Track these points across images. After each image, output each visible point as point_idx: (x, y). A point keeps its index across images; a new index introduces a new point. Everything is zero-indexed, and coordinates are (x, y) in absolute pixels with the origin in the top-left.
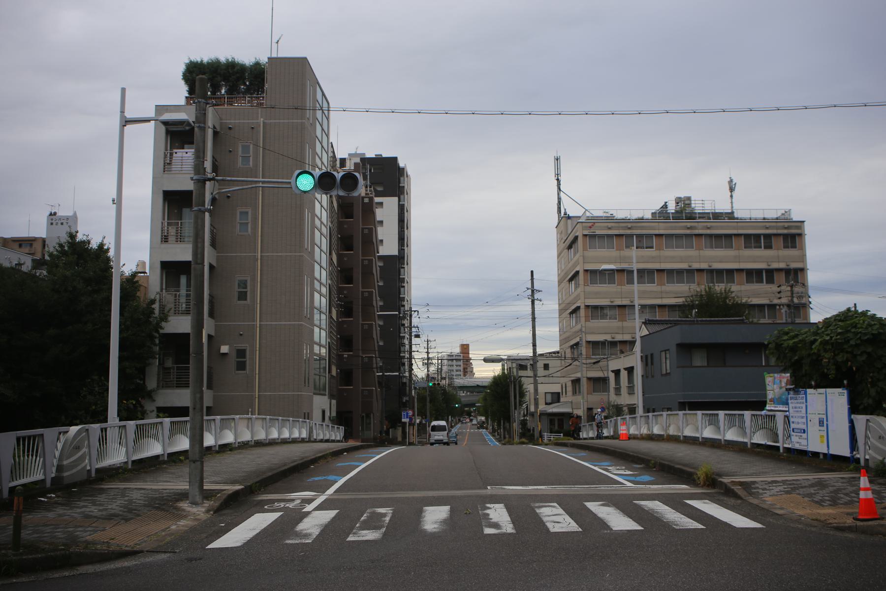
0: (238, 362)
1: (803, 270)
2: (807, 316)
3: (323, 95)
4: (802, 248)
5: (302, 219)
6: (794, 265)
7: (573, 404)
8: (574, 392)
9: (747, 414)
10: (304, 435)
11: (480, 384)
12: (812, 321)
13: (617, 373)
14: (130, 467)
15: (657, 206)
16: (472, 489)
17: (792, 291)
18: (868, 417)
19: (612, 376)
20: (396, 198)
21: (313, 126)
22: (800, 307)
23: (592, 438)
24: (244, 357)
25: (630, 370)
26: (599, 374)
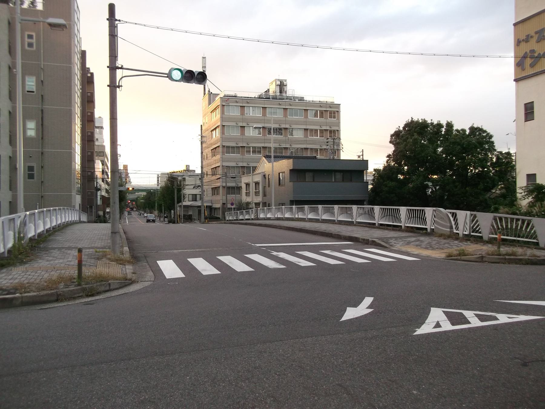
0: (28, 174)
1: (338, 131)
2: (339, 155)
3: (78, 7)
4: (339, 119)
5: (70, 86)
6: (334, 128)
7: (217, 202)
8: (213, 194)
9: (354, 207)
10: (235, 218)
11: (139, 188)
12: (341, 159)
13: (247, 185)
14: (36, 238)
15: (262, 91)
16: (300, 246)
17: (334, 142)
18: (434, 208)
19: (244, 186)
20: (203, 86)
21: (74, 25)
22: (337, 150)
23: (252, 219)
24: (33, 171)
25: (257, 184)
26: (232, 184)
